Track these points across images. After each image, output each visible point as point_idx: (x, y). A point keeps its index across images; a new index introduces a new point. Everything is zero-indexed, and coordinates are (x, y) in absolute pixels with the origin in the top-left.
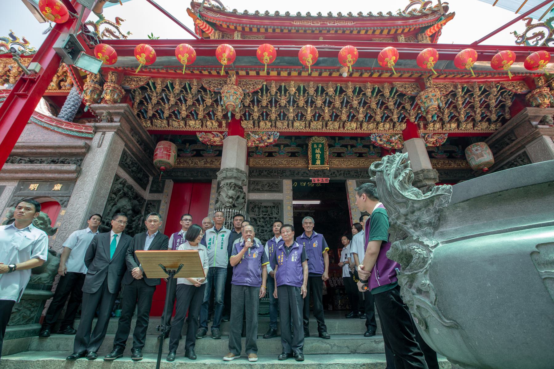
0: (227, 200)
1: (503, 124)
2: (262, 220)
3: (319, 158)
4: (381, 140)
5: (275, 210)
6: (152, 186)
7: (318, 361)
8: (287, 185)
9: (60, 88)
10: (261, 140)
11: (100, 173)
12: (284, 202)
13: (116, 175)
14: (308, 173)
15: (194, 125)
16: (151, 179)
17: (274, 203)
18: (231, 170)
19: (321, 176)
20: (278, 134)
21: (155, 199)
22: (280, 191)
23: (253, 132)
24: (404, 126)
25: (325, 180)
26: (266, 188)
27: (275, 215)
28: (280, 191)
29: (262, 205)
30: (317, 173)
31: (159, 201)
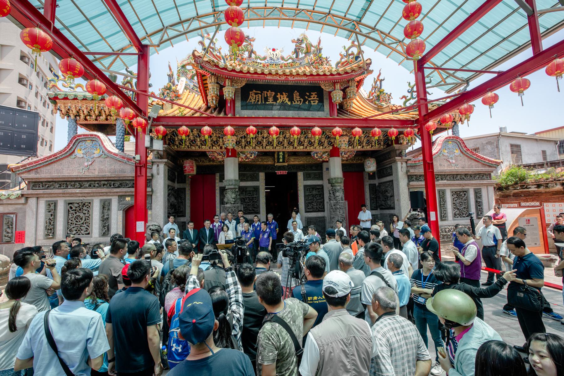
0: (231, 200)
1: (387, 147)
6: (178, 179)
8: (262, 175)
9: (107, 119)
10: (246, 157)
13: (305, 314)
14: (273, 167)
15: (204, 149)
16: (176, 174)
18: (232, 180)
19: (282, 170)
22: (258, 180)
23: (241, 152)
24: (331, 148)
25: (285, 172)
26: (249, 179)
27: (255, 196)
28: (258, 180)
30: (280, 168)
31: (185, 189)
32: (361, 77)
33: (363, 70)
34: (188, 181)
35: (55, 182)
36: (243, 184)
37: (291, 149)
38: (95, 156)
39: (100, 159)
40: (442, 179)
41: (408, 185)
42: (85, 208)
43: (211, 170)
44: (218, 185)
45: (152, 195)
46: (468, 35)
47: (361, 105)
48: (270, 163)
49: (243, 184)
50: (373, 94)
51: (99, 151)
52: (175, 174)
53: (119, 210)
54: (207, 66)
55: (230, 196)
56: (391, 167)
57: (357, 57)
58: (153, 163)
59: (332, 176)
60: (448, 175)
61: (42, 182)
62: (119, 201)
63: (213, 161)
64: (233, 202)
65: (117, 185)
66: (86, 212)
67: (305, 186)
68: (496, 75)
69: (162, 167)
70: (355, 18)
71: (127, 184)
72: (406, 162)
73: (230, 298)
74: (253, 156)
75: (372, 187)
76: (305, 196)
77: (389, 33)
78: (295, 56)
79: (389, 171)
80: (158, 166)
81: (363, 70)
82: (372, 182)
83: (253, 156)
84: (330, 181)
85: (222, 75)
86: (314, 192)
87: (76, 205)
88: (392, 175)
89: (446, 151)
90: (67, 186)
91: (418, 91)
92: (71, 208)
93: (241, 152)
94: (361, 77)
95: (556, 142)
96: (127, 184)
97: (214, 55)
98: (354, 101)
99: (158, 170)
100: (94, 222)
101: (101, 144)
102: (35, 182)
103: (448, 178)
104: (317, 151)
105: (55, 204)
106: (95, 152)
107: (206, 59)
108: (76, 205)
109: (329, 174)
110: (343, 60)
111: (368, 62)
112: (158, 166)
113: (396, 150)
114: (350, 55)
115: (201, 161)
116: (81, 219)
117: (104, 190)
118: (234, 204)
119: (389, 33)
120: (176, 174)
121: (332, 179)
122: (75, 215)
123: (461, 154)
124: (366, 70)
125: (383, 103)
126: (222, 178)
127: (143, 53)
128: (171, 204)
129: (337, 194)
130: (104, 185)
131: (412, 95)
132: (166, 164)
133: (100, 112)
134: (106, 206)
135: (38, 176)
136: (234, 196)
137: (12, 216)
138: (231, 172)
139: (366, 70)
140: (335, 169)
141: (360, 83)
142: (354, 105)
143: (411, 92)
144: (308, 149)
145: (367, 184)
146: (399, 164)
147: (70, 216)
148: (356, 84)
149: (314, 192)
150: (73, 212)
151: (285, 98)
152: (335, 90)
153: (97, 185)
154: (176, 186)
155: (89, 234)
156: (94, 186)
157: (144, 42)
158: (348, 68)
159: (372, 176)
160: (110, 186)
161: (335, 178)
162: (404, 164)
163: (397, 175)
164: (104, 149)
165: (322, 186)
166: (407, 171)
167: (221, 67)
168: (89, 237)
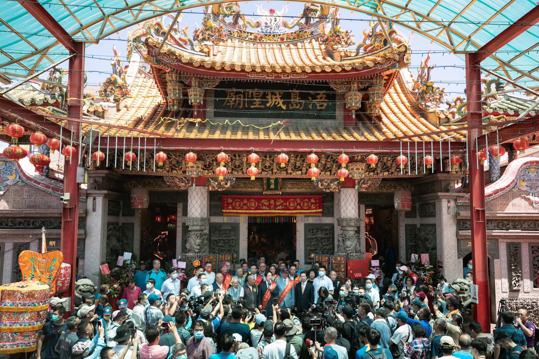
0: (195, 247)
2: (222, 241)
3: (273, 183)
4: (322, 185)
5: (232, 233)
7: (475, 175)
10: (219, 185)
11: (101, 234)
12: (241, 225)
16: (121, 203)
17: (232, 227)
20: (234, 179)
21: (128, 222)
23: (212, 178)
29: (222, 228)
31: (133, 224)
33: (393, 62)
34: (138, 215)
36: (216, 220)
37: (283, 175)
38: (8, 182)
39: (16, 187)
40: (515, 228)
43: (169, 203)
45: (85, 240)
48: (256, 190)
49: (216, 220)
51: (14, 176)
52: (118, 205)
54: (165, 59)
55: (194, 242)
56: (434, 203)
58: (87, 195)
59: (343, 215)
60: (525, 221)
64: (197, 251)
65: (38, 225)
67: (306, 226)
69: (100, 201)
71: (51, 223)
72: (456, 200)
73: (380, 272)
74: (229, 184)
76: (306, 239)
77: (428, 15)
80: (94, 199)
81: (393, 62)
82: (410, 221)
83: (229, 184)
84: (340, 221)
86: (320, 235)
89: (525, 184)
93: (212, 178)
97: (176, 41)
99: (94, 205)
101: (18, 169)
104: (323, 178)
106: (10, 177)
107: (165, 49)
110: (368, 42)
112: (94, 199)
113: (441, 181)
115: (157, 184)
117: (20, 231)
118: (198, 253)
119: (428, 15)
120: (121, 203)
121: (343, 220)
124: (399, 62)
125: (429, 104)
126: (185, 213)
127: (76, 49)
128: (111, 250)
129: (348, 243)
130: (20, 223)
132: (106, 196)
136: (198, 241)
138: (197, 206)
139: (399, 62)
140: (349, 206)
146: (444, 204)
148: (384, 82)
149: (320, 235)
152: (350, 90)
153: (10, 224)
154: (122, 220)
156: (7, 225)
157: (78, 37)
160: (29, 225)
161: (346, 220)
162: (452, 204)
163: (441, 219)
164: (21, 174)
166: (457, 214)
167: (184, 61)
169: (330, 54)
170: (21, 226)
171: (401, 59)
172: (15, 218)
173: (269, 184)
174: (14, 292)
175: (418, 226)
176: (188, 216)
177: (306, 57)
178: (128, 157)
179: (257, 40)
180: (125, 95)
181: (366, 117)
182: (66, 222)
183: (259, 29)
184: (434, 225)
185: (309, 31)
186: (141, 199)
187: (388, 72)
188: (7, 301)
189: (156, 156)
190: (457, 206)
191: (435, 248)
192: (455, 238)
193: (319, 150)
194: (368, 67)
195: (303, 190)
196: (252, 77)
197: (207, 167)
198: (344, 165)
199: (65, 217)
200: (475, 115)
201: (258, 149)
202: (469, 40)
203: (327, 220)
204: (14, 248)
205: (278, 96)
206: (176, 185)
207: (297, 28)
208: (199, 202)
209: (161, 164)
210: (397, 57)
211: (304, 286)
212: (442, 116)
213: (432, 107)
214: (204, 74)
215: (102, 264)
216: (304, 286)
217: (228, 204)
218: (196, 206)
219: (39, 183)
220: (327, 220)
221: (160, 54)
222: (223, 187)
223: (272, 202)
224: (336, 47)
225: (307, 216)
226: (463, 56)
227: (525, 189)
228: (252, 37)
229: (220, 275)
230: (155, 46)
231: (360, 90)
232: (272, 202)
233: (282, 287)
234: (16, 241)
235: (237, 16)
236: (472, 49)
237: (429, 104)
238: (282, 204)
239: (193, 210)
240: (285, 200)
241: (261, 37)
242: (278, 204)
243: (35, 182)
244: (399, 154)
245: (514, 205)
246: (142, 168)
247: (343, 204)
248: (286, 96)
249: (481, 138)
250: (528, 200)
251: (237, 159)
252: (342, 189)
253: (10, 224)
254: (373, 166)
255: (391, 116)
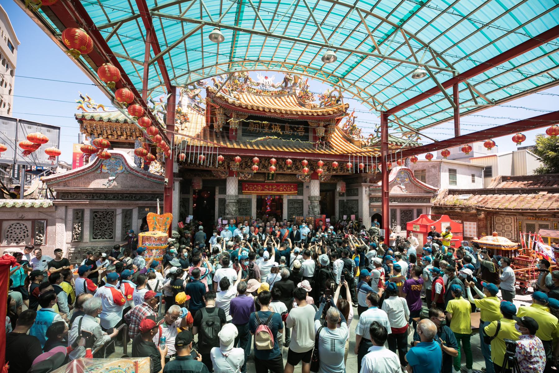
23: (241, 172)
31: (189, 199)
32: (340, 117)
35: (82, 193)
36: (241, 197)
38: (118, 171)
39: (123, 175)
41: (370, 205)
42: (108, 216)
44: (218, 196)
46: (420, 104)
47: (338, 143)
48: (261, 180)
49: (241, 197)
50: (346, 126)
51: (122, 167)
53: (139, 219)
54: (218, 100)
57: (338, 101)
59: (312, 194)
61: (70, 193)
62: (139, 212)
63: (217, 177)
66: (110, 220)
67: (289, 200)
68: (433, 142)
70: (340, 75)
71: (146, 197)
72: (369, 187)
75: (341, 202)
76: (288, 208)
78: (284, 85)
79: (356, 192)
82: (341, 198)
84: (310, 198)
85: (230, 109)
87: (101, 214)
88: (358, 195)
90: (93, 197)
91: (382, 132)
92: (96, 216)
94: (340, 117)
95: (483, 168)
96: (146, 197)
98: (333, 135)
100: (117, 228)
101: (124, 163)
102: (63, 193)
103: (399, 200)
105: (83, 211)
106: (119, 168)
107: (219, 94)
108: (101, 214)
109: (309, 192)
111: (347, 106)
114: (332, 97)
116: (106, 225)
117: (127, 202)
121: (312, 197)
122: (100, 222)
123: (410, 183)
125: (354, 136)
131: (377, 135)
133: (122, 133)
134: (127, 215)
135: (66, 188)
137: (43, 221)
141: (338, 121)
142: (332, 139)
143: (377, 131)
144: (294, 172)
145: (338, 199)
146: (364, 189)
147: (95, 223)
149: (296, 206)
150: (98, 219)
151: (278, 129)
153: (120, 197)
155: (112, 238)
158: (330, 110)
159: (341, 195)
161: (314, 197)
162: (367, 189)
164: (127, 167)
165: (302, 200)
166: (370, 194)
168: (112, 241)
169: (302, 105)
170: (127, 199)
171: (343, 113)
172: (123, 194)
173: (268, 177)
174: (150, 237)
175: (345, 201)
176: (227, 194)
177: (288, 105)
178: (200, 158)
179: (257, 93)
180: (186, 120)
181: (325, 141)
182: (166, 196)
183: (259, 87)
184: (358, 200)
185: (287, 91)
186: (198, 185)
187: (338, 118)
188: (147, 242)
189: (218, 157)
190: (370, 190)
191: (357, 212)
192: (368, 207)
193: (308, 158)
194: (330, 114)
195: (286, 180)
196: (268, 114)
197: (264, 167)
198: (321, 167)
199: (166, 193)
200: (384, 144)
201: (276, 156)
202: (383, 104)
203: (300, 197)
204: (123, 213)
205: (278, 127)
206: (219, 176)
207: (280, 89)
208: (234, 186)
209: (221, 162)
210: (344, 111)
211: (295, 233)
212: (363, 143)
213: (356, 138)
214: (241, 111)
215: (179, 222)
216: (295, 233)
217: (246, 188)
218: (232, 188)
219: (138, 172)
220: (300, 197)
221: (215, 97)
222: (246, 178)
223: (270, 187)
224: (306, 101)
225: (289, 195)
226: (380, 112)
227: (399, 182)
228: (255, 91)
229: (253, 228)
230: (213, 92)
231: (324, 126)
232: (270, 187)
233: (283, 234)
234: (124, 208)
235: (246, 79)
236: (384, 110)
237: (354, 136)
238: (276, 188)
239: (230, 191)
240: (278, 186)
241: (261, 92)
242: (274, 188)
243: (136, 171)
244: (348, 162)
245: (394, 190)
246: (209, 165)
247: (312, 188)
248: (283, 128)
249: (389, 155)
250: (400, 187)
251: (265, 161)
252: (312, 180)
253: (120, 197)
254: (335, 168)
255: (335, 141)
